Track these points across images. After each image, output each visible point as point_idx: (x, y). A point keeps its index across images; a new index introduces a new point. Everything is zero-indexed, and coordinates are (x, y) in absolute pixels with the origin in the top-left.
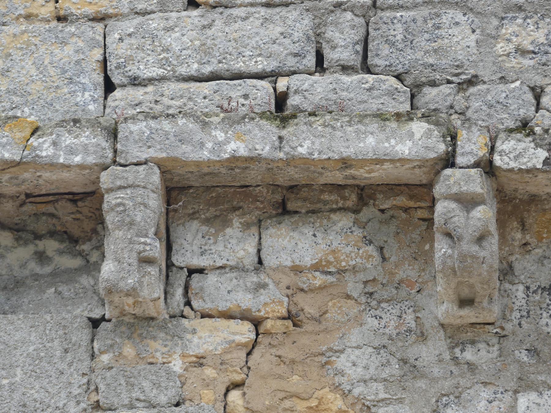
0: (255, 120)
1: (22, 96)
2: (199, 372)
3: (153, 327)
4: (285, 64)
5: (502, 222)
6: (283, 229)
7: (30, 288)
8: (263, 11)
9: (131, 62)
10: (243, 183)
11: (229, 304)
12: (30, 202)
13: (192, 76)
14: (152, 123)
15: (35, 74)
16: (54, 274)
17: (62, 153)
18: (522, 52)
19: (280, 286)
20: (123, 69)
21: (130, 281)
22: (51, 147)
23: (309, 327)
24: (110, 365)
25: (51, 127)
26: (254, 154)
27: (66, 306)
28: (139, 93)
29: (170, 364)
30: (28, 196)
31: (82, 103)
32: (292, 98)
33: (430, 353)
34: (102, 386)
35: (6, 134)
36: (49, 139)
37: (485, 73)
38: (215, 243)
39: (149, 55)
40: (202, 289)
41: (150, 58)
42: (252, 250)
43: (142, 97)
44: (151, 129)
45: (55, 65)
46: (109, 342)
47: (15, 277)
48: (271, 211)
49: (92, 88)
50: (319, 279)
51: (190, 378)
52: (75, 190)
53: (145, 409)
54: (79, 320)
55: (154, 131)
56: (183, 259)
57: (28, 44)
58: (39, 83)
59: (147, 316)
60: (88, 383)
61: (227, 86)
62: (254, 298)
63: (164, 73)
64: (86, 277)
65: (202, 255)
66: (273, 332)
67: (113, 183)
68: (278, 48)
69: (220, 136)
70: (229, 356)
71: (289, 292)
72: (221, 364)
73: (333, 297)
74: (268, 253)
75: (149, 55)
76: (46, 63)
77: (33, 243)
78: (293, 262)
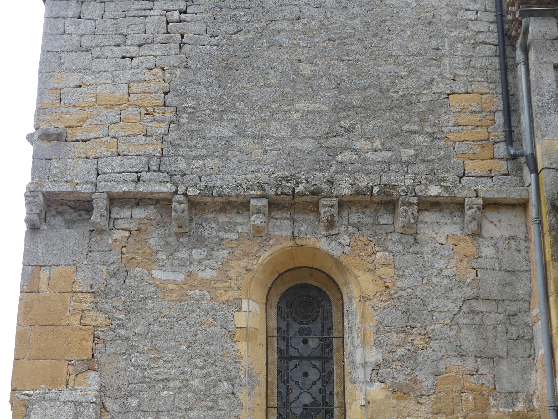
5: (190, 208)
6: (137, 209)
8: (135, 157)
16: (83, 219)
18: (197, 168)
23: (143, 232)
33: (172, 239)
37: (188, 173)
42: (130, 214)
50: (145, 221)
57: (79, 164)
69: (122, 186)
73: (149, 225)
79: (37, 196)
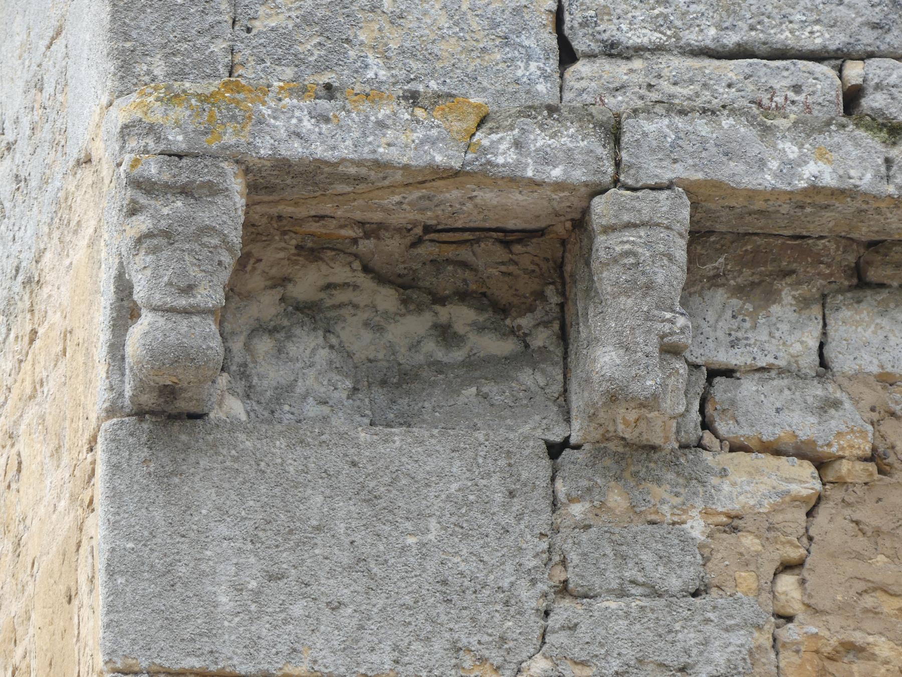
0: (847, 129)
1: (426, 60)
2: (733, 541)
3: (656, 462)
4: (859, 40)
6: (864, 312)
7: (433, 385)
9: (606, 17)
10: (798, 231)
11: (778, 431)
12: (432, 241)
13: (706, 47)
14: (679, 122)
15: (447, 25)
17: (530, 161)
19: (860, 405)
20: (593, 28)
21: (649, 383)
22: (512, 150)
24: (587, 522)
25: (510, 116)
26: (848, 184)
27: (504, 418)
28: (620, 69)
29: (684, 526)
30: (427, 229)
31: (525, 79)
32: (871, 97)
34: (574, 557)
35: (437, 122)
36: (510, 136)
38: (754, 327)
39: (635, 8)
40: (733, 403)
41: (638, 13)
43: (625, 77)
44: (677, 131)
45: (479, 13)
46: (585, 483)
47: (400, 364)
48: (842, 280)
49: (542, 56)
51: (718, 551)
52: (511, 224)
53: (643, 598)
54: (531, 443)
55: (682, 135)
56: (702, 351)
58: (453, 41)
59: (645, 442)
60: (550, 550)
61: (764, 69)
62: (819, 423)
63: (661, 39)
64: (531, 371)
65: (732, 346)
66: (849, 481)
67: (616, 216)
68: (847, 12)
69: (792, 151)
70: (779, 517)
71: (875, 416)
72: (769, 529)
74: (839, 349)
75: (635, 8)
76: (464, 8)
77: (431, 309)
78: (882, 367)
79: (214, 190)
